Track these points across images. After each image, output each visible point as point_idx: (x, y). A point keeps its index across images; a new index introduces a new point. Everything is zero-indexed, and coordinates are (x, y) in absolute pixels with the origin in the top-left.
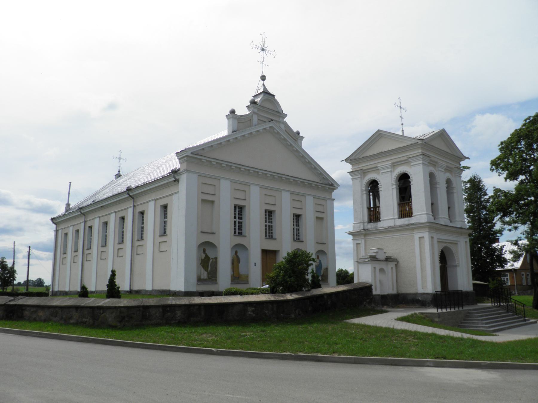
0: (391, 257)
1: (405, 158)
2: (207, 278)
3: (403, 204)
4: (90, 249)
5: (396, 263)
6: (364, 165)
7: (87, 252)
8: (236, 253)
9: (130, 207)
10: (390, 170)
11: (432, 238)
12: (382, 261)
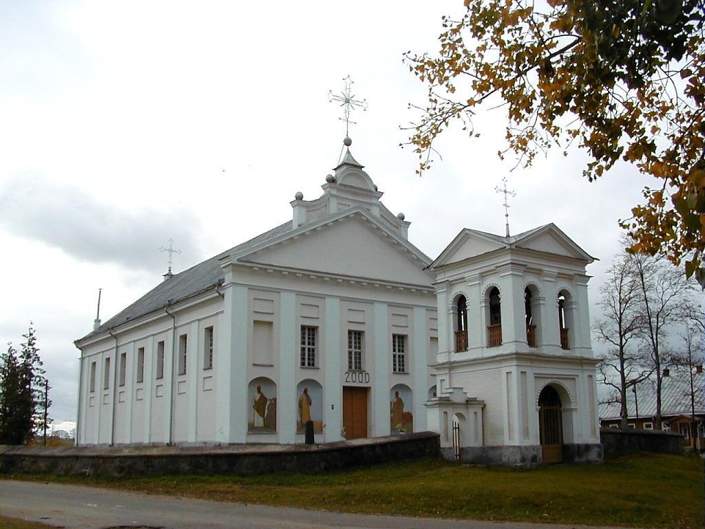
0: (476, 398)
1: (493, 267)
4: (124, 385)
5: (482, 406)
7: (120, 389)
8: (306, 391)
11: (523, 373)
12: (460, 404)
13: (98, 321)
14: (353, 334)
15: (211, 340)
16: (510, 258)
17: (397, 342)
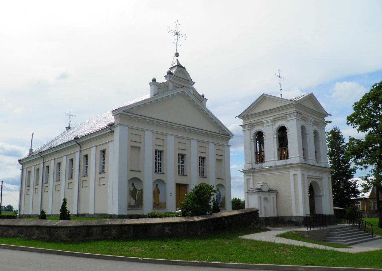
0: (272, 189)
1: (283, 115)
2: (135, 205)
3: (281, 149)
4: (38, 185)
6: (252, 120)
7: (45, 185)
8: (157, 186)
9: (77, 152)
10: (272, 124)
12: (266, 192)
13: (31, 150)
14: (180, 155)
15: (72, 165)
16: (295, 109)
17: (201, 161)
